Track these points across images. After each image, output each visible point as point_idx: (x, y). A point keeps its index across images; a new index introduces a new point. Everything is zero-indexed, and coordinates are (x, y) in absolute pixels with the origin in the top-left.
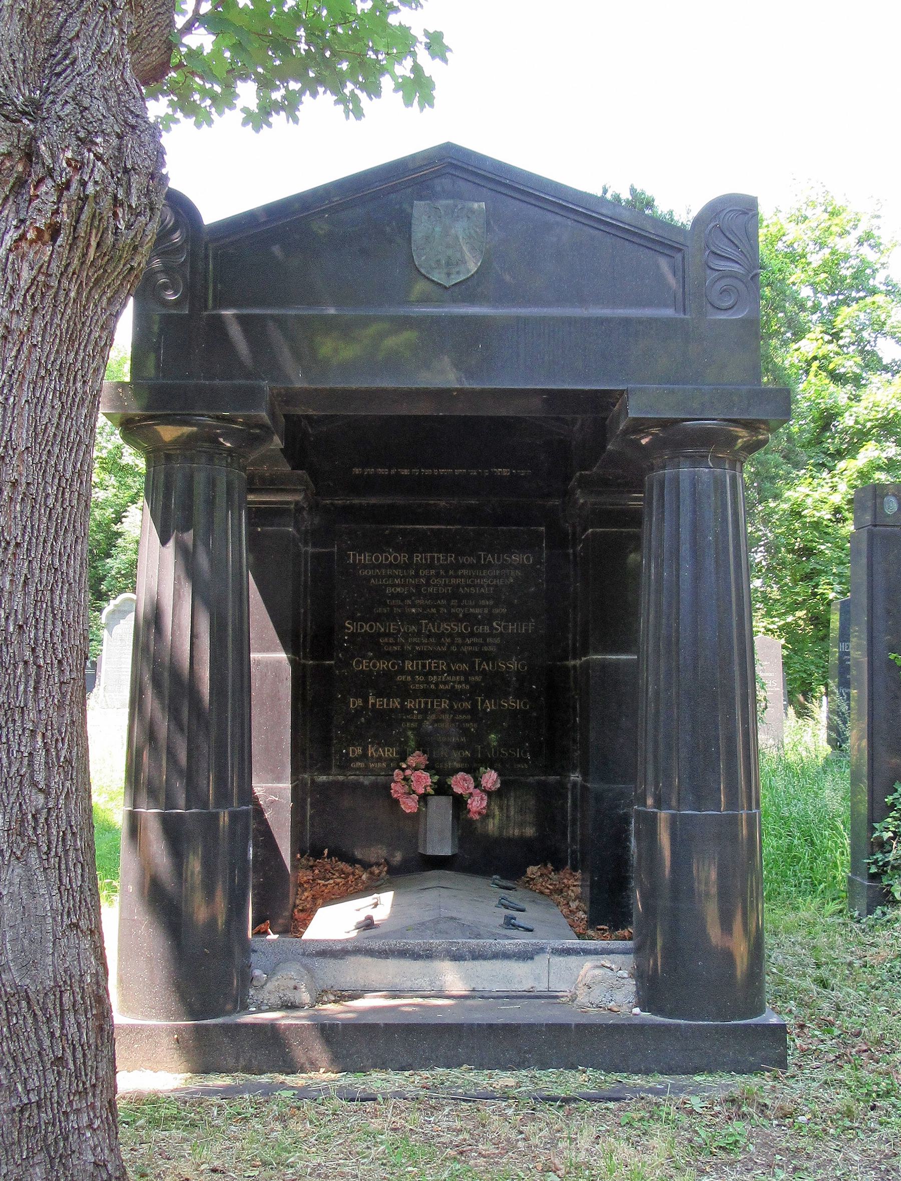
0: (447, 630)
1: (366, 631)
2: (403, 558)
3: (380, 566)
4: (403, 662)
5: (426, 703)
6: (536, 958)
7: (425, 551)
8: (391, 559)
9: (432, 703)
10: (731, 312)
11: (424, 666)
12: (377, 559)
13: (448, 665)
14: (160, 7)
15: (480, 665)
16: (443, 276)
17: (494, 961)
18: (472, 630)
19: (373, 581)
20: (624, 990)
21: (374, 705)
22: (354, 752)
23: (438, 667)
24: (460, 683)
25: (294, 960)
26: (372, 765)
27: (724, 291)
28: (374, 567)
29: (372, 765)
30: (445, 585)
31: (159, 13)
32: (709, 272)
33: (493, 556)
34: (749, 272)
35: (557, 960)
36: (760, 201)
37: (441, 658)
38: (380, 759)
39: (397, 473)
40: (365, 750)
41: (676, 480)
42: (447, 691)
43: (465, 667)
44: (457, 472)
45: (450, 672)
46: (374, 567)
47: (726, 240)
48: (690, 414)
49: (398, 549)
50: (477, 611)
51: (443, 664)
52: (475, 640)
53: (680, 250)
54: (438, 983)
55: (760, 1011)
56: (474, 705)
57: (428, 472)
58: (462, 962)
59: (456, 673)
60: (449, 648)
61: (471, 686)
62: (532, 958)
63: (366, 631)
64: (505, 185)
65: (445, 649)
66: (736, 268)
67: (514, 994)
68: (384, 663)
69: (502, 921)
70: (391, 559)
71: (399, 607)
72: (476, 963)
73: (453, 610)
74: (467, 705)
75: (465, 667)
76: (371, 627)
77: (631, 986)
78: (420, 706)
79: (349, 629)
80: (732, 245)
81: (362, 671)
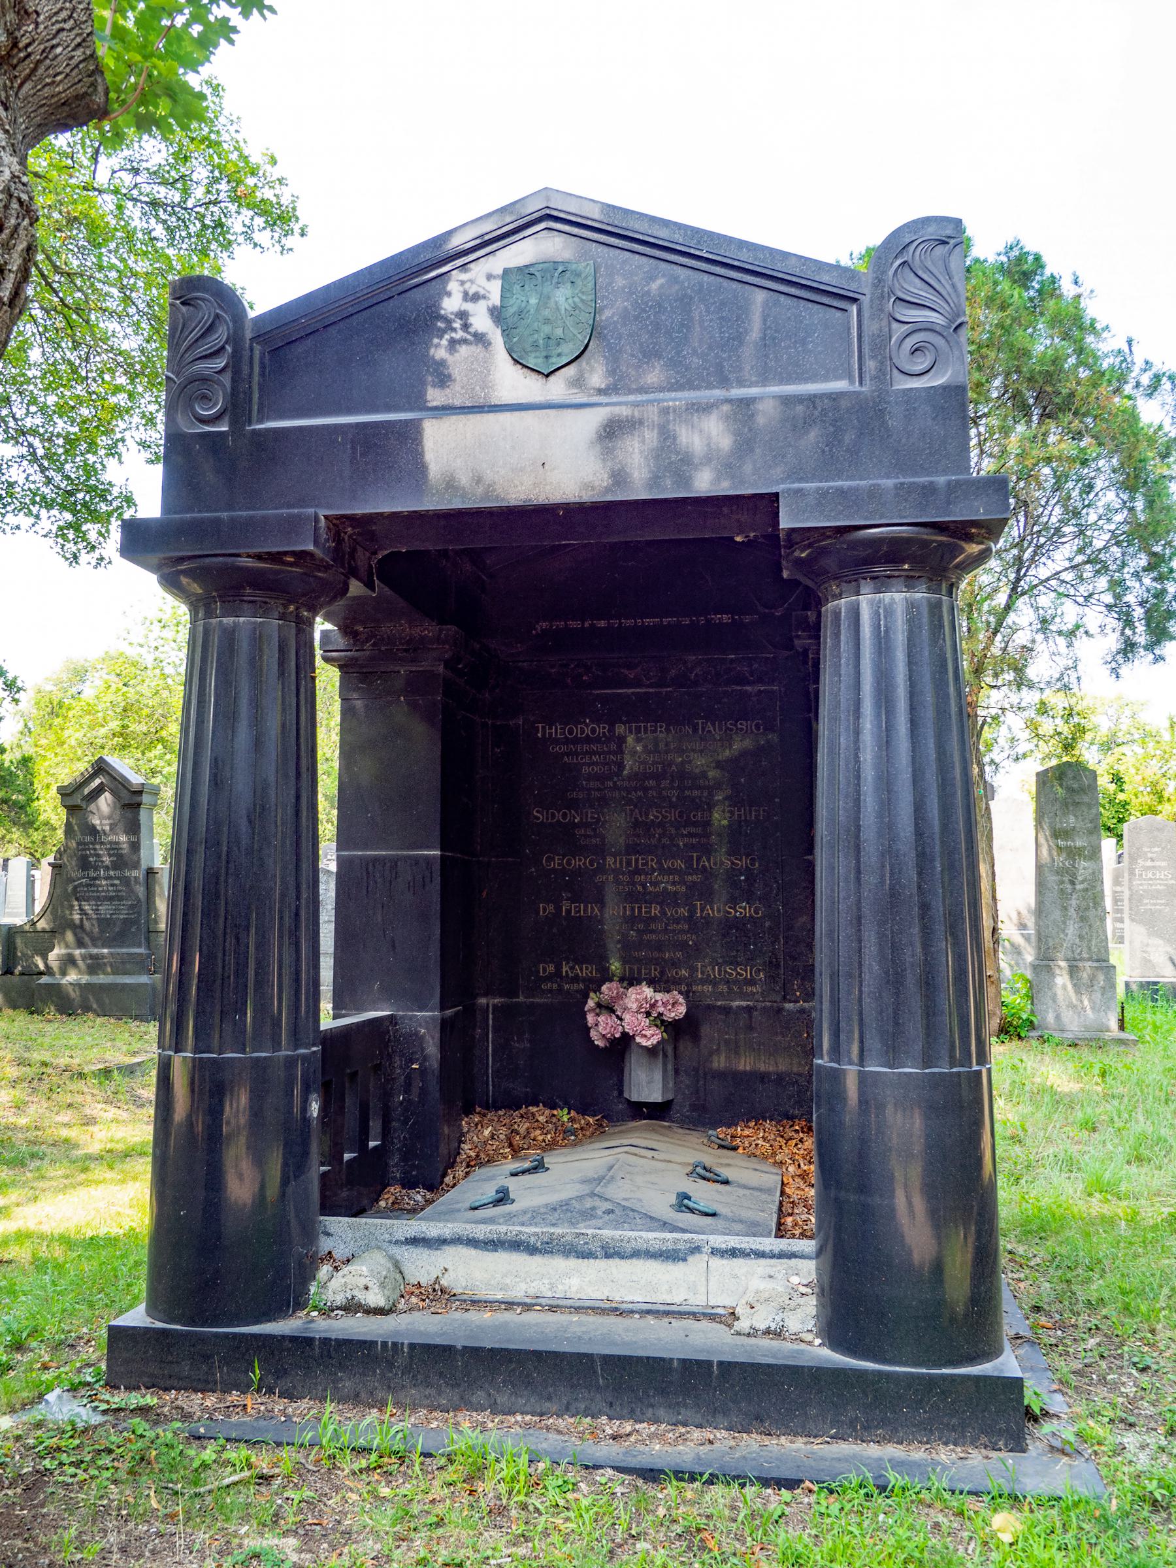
0: (657, 817)
1: (558, 821)
2: (602, 729)
3: (576, 741)
4: (604, 859)
5: (633, 909)
6: (690, 1259)
7: (628, 722)
8: (588, 731)
9: (640, 908)
10: (926, 377)
11: (629, 863)
12: (571, 732)
13: (659, 862)
14: (65, 21)
15: (698, 859)
16: (540, 360)
17: (634, 1261)
18: (688, 817)
19: (566, 759)
20: (800, 1313)
21: (569, 911)
22: (544, 970)
23: (646, 864)
24: (674, 883)
25: (379, 1248)
26: (567, 987)
27: (916, 350)
28: (567, 741)
29: (567, 987)
30: (654, 763)
31: (63, 29)
32: (895, 325)
33: (713, 725)
34: (951, 321)
35: (717, 1263)
36: (966, 222)
37: (650, 852)
38: (576, 979)
39: (592, 625)
40: (558, 968)
41: (855, 613)
42: (657, 895)
43: (680, 864)
44: (665, 621)
45: (662, 870)
46: (567, 741)
47: (917, 280)
48: (866, 518)
49: (598, 720)
50: (696, 793)
51: (652, 860)
52: (693, 830)
53: (855, 300)
54: (560, 1287)
55: (991, 1351)
56: (692, 912)
57: (629, 623)
58: (592, 1261)
59: (671, 871)
60: (659, 840)
61: (689, 888)
62: (685, 1260)
63: (558, 821)
64: (733, 267)
65: (654, 841)
66: (933, 316)
67: (662, 1308)
68: (580, 860)
69: (673, 1199)
70: (588, 731)
71: (599, 790)
72: (610, 1262)
73: (687, 793)
74: (683, 912)
75: (680, 864)
76: (564, 816)
77: (810, 1306)
78: (625, 913)
79: (538, 818)
80: (932, 291)
81: (554, 870)
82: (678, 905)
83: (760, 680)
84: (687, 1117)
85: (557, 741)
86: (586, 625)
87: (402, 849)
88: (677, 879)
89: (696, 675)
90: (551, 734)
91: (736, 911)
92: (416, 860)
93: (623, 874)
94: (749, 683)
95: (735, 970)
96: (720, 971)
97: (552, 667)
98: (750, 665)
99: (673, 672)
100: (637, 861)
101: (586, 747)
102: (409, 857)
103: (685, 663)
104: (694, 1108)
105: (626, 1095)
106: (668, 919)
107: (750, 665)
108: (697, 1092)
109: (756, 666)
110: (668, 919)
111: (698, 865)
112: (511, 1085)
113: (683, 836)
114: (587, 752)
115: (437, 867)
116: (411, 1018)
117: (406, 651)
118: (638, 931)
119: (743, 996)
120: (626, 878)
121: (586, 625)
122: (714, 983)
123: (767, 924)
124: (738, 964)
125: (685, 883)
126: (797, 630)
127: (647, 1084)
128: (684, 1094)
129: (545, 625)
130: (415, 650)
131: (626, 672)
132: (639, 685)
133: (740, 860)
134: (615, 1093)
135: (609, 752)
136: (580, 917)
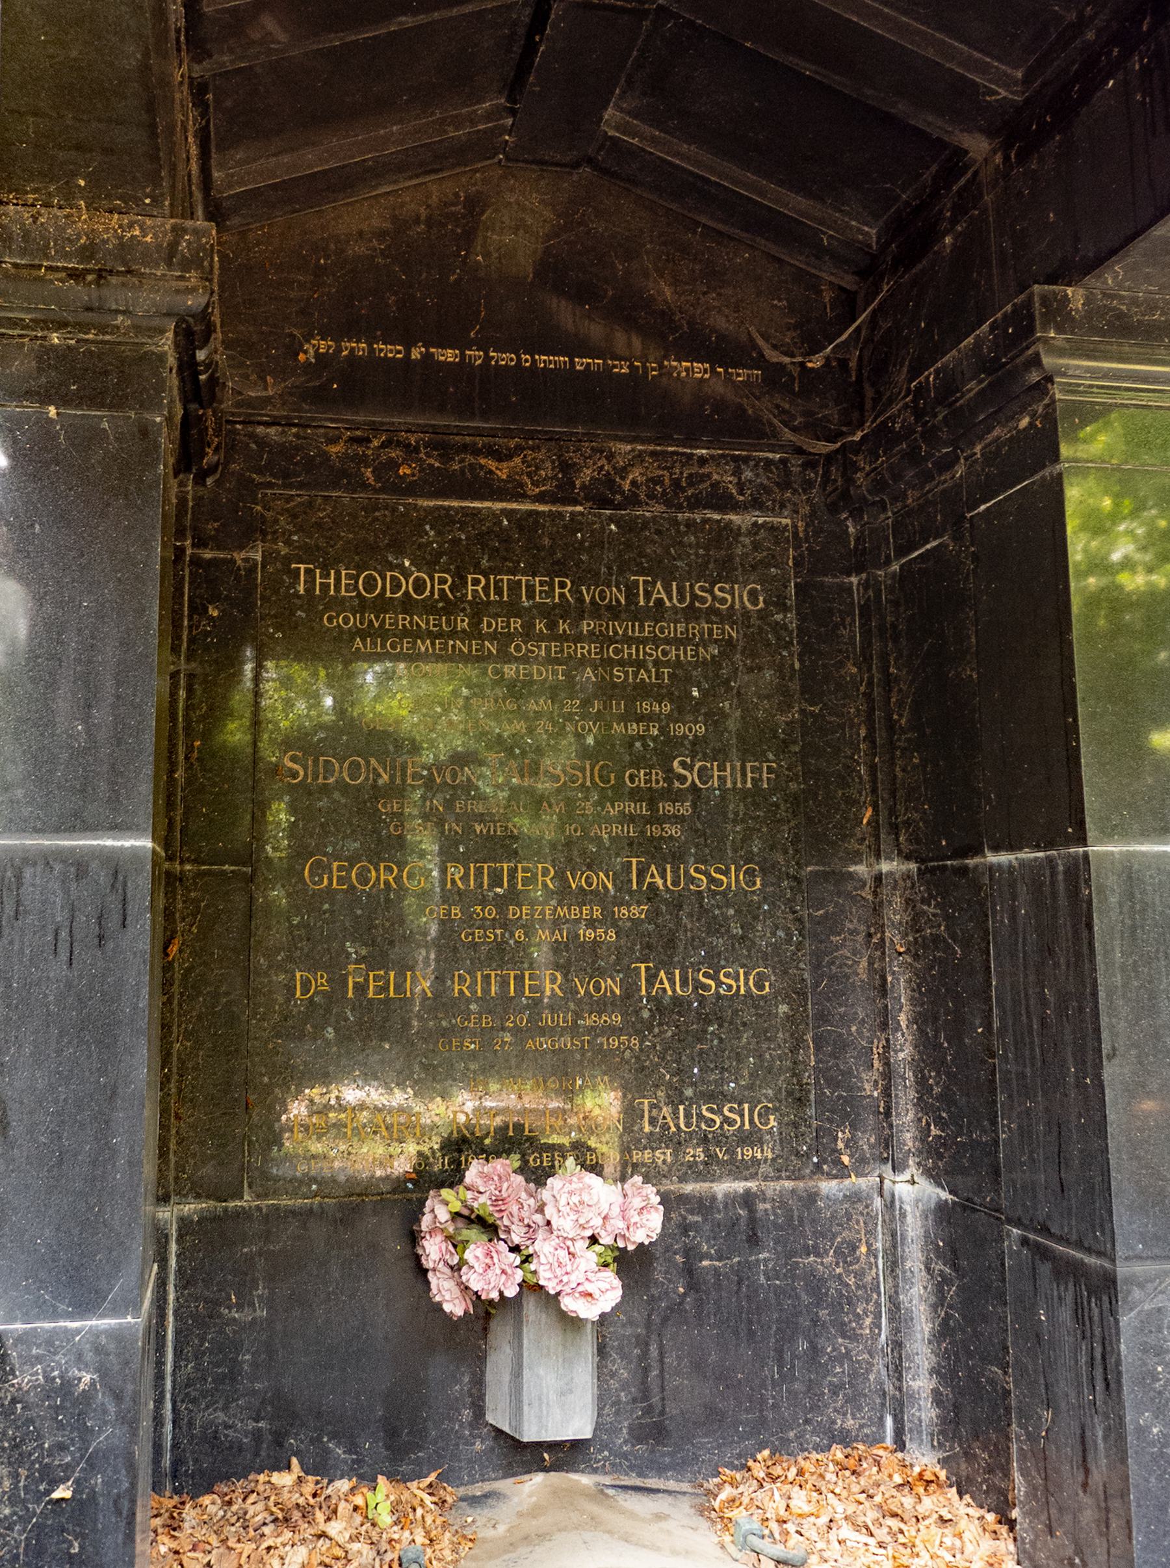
3: (382, 605)
5: (504, 983)
8: (407, 586)
11: (496, 880)
12: (370, 584)
15: (641, 874)
24: (592, 924)
28: (362, 606)
39: (427, 356)
44: (580, 363)
46: (362, 606)
49: (430, 563)
56: (630, 991)
57: (506, 359)
70: (407, 586)
74: (612, 985)
75: (603, 880)
76: (355, 769)
78: (486, 991)
79: (294, 775)
81: (329, 892)
82: (602, 973)
83: (756, 504)
84: (625, 1456)
85: (338, 604)
86: (415, 354)
87: (57, 830)
88: (597, 914)
89: (634, 483)
90: (325, 587)
91: (719, 984)
92: (79, 865)
93: (483, 902)
94: (735, 507)
95: (719, 1112)
96: (688, 1115)
97: (333, 441)
98: (737, 472)
99: (587, 475)
100: (513, 872)
101: (403, 621)
102: (62, 855)
103: (610, 457)
104: (638, 1435)
105: (498, 1417)
106: (579, 1002)
107: (737, 472)
108: (645, 1394)
109: (748, 474)
110: (579, 1002)
111: (640, 882)
112: (221, 1416)
113: (609, 820)
114: (405, 633)
115: (141, 885)
116: (50, 1341)
117: (75, 275)
118: (516, 1031)
119: (739, 1170)
120: (491, 912)
121: (415, 354)
122: (678, 1143)
123: (783, 1008)
124: (727, 1098)
125: (615, 924)
126: (1045, 329)
127: (556, 1396)
128: (618, 1402)
129: (324, 345)
130: (101, 274)
131: (492, 464)
132: (522, 497)
133: (726, 873)
134: (467, 1414)
135: (453, 634)
136: (388, 1001)
